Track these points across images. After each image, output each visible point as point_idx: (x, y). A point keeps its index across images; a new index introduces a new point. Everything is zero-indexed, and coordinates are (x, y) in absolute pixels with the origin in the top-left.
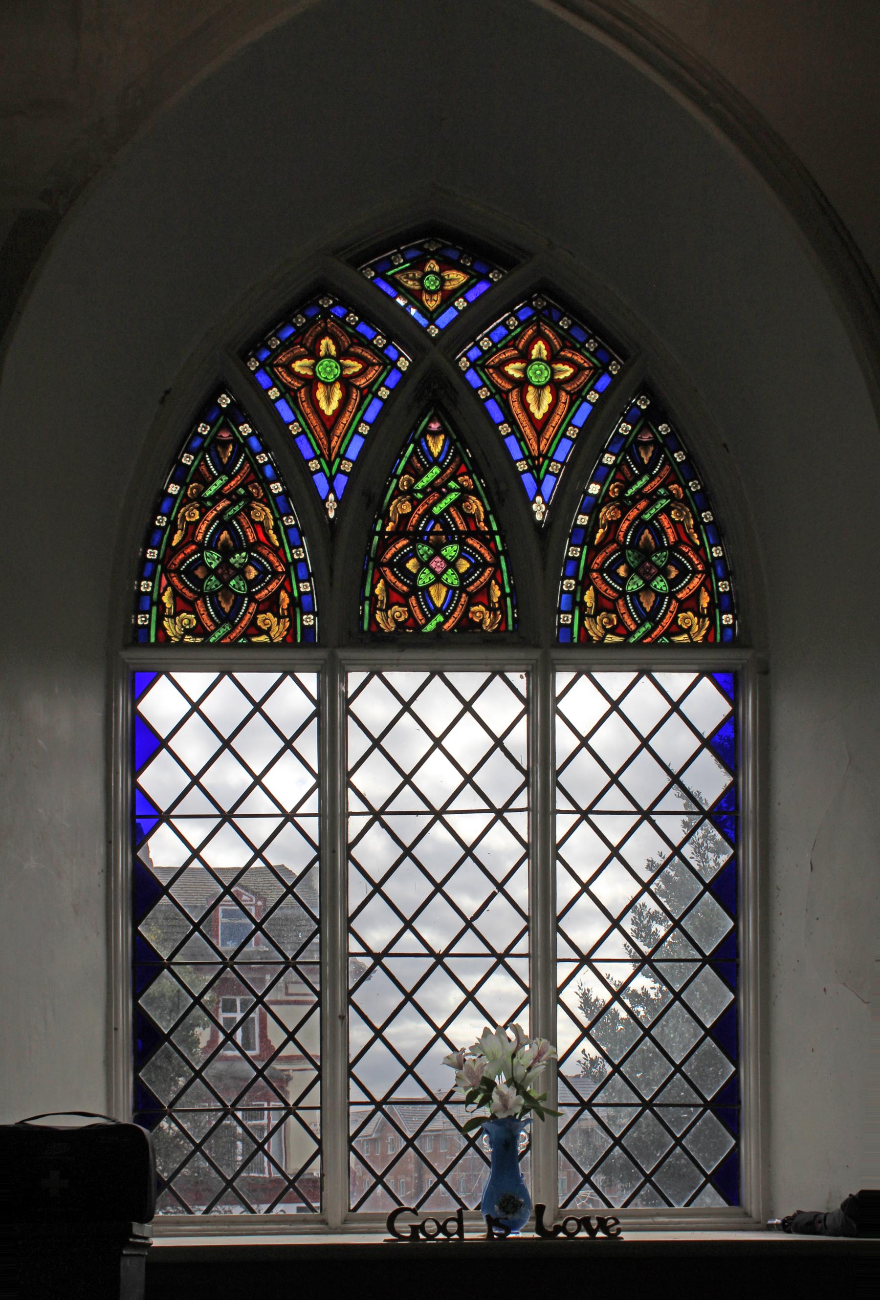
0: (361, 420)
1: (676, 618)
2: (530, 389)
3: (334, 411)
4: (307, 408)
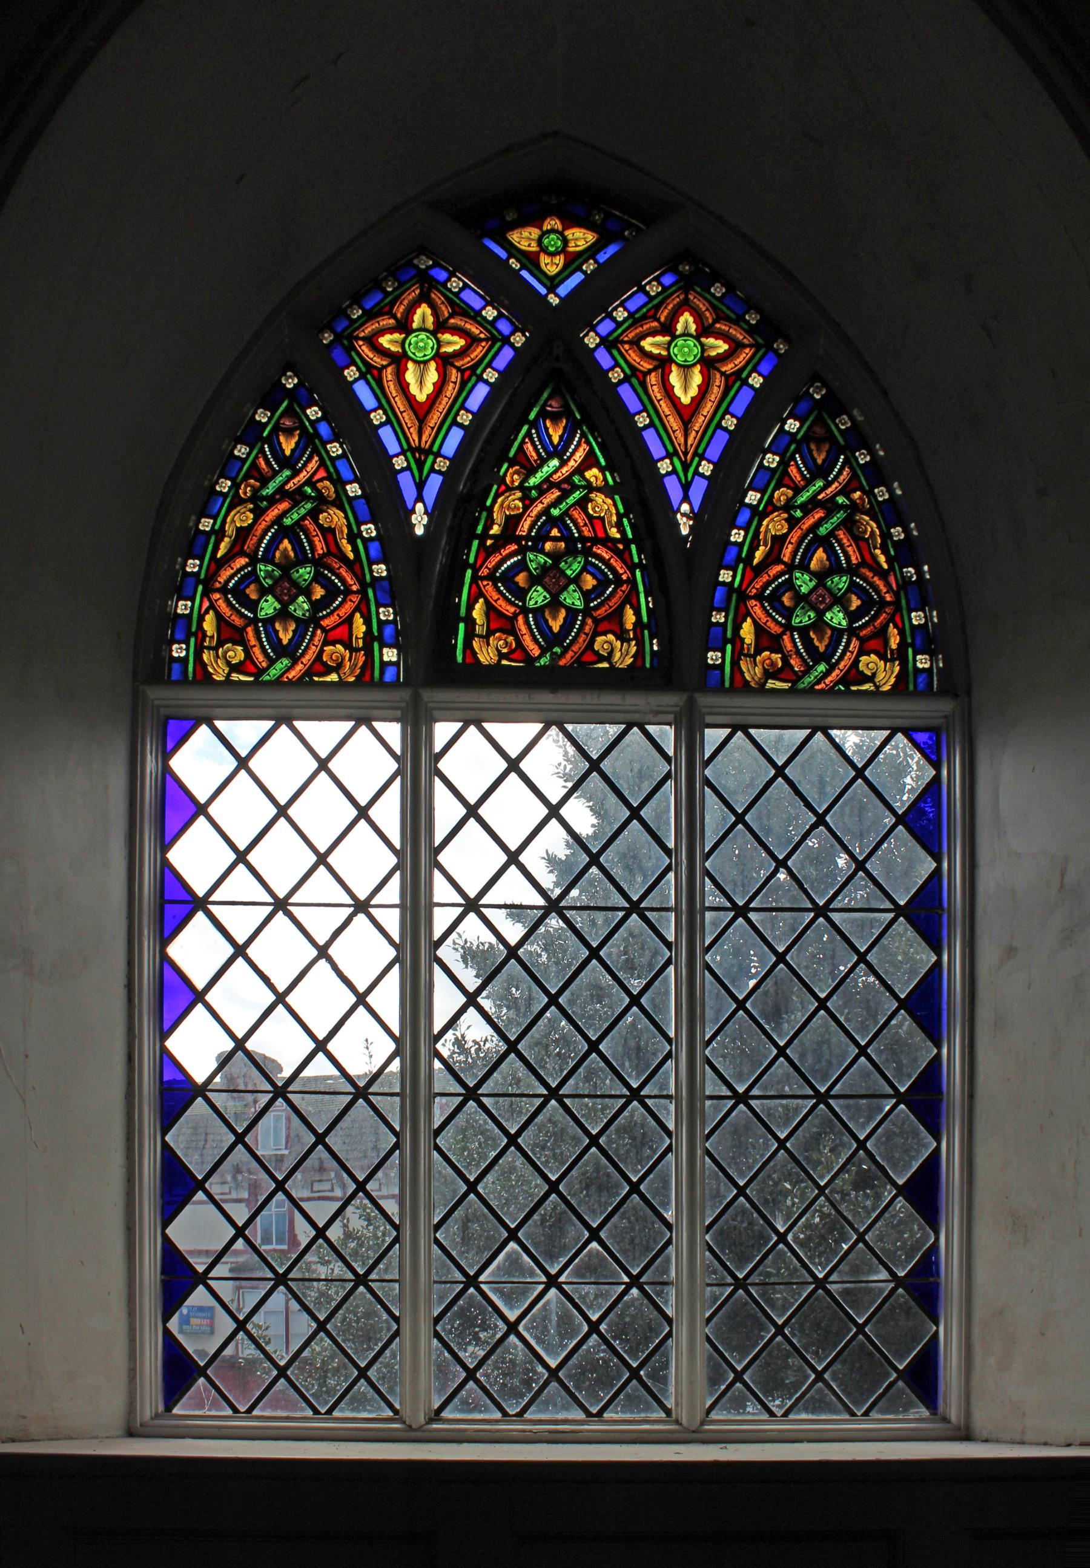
0: (727, 412)
1: (856, 662)
2: (410, 365)
3: (693, 398)
4: (392, 388)
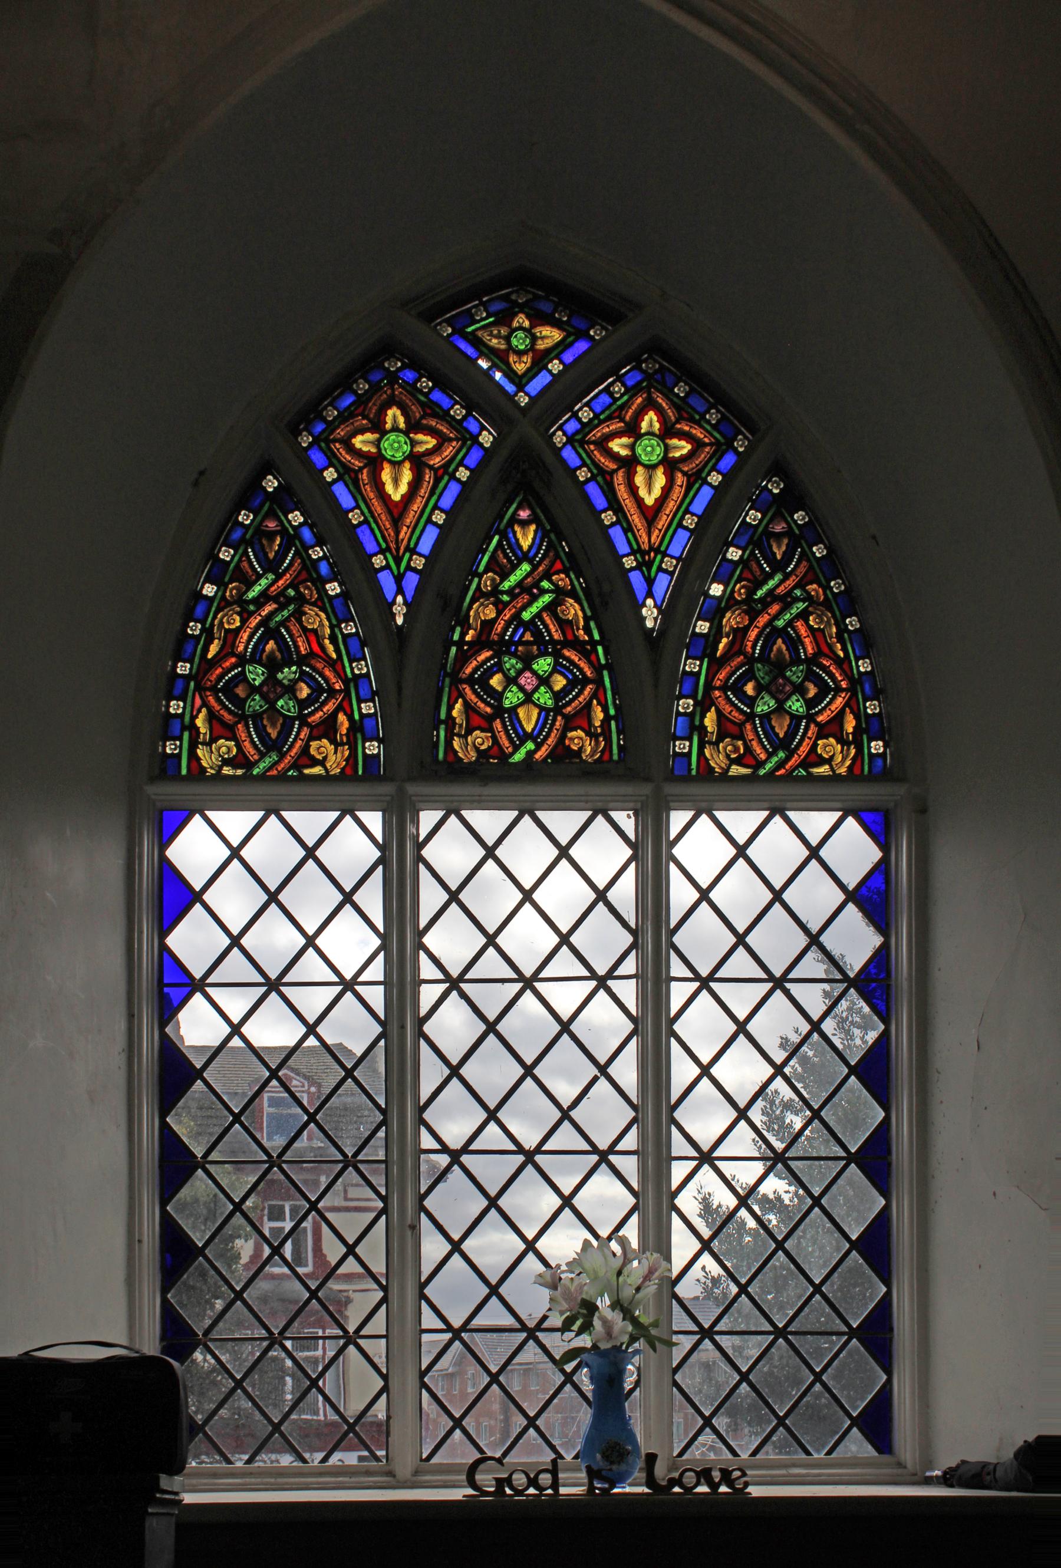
0: (436, 507)
1: (815, 746)
2: (639, 469)
3: (402, 496)
4: (370, 493)
